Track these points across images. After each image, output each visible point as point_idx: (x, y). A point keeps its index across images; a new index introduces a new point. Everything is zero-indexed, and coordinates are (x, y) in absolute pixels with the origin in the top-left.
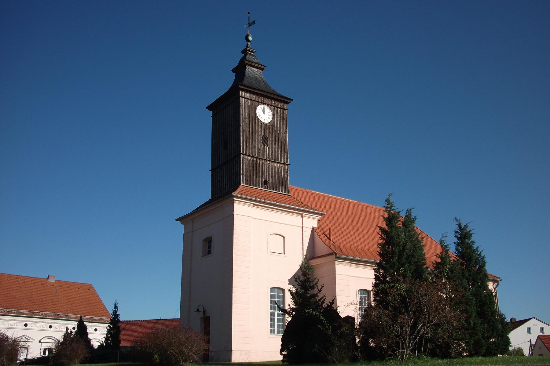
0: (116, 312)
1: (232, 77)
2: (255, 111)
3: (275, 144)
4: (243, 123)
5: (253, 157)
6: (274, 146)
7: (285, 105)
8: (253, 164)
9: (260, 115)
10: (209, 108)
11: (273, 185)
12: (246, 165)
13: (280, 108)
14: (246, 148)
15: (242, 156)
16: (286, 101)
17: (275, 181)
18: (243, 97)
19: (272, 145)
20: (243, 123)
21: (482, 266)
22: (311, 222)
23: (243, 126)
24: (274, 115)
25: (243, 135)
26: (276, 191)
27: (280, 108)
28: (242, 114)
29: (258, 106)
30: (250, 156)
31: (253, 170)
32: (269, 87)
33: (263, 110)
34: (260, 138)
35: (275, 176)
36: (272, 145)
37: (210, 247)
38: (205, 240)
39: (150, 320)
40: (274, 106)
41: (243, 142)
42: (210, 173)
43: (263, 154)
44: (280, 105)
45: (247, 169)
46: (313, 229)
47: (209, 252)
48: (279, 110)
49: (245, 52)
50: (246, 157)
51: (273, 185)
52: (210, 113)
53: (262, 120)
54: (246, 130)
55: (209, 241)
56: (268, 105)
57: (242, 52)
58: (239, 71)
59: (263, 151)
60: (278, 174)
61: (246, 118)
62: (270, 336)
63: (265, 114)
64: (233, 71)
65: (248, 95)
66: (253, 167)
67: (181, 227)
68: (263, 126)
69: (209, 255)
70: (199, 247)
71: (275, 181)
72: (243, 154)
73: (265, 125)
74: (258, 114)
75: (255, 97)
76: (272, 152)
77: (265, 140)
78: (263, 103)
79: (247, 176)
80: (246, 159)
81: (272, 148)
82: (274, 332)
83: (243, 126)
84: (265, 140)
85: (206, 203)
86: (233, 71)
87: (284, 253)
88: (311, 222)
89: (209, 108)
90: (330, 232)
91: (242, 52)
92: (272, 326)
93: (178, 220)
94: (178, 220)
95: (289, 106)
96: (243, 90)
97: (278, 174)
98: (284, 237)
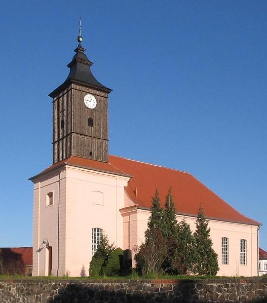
1: (66, 72)
16: (108, 91)
35: (98, 149)
44: (102, 94)
56: (93, 94)
57: (75, 51)
58: (72, 65)
63: (90, 101)
64: (69, 66)
65: (78, 87)
74: (85, 102)
75: (84, 89)
77: (91, 122)
78: (89, 93)
84: (91, 122)
86: (69, 66)
96: (74, 83)
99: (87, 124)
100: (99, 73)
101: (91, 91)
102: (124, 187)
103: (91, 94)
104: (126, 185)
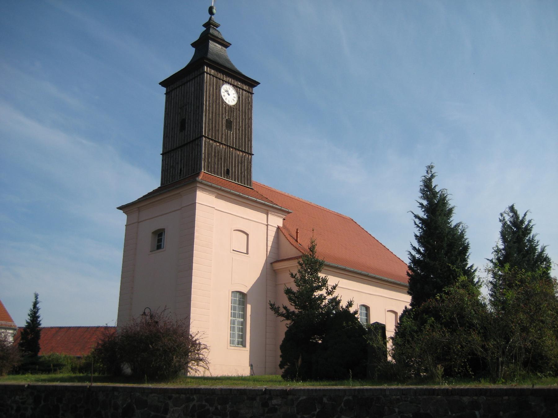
0: (35, 313)
1: (191, 52)
2: (220, 90)
3: (239, 130)
4: (206, 102)
5: (215, 141)
6: (238, 132)
7: (251, 89)
8: (215, 149)
9: (224, 96)
10: (163, 84)
11: (235, 175)
12: (208, 150)
13: (245, 91)
14: (209, 130)
15: (204, 139)
16: (252, 83)
17: (238, 171)
18: (207, 73)
19: (236, 131)
20: (206, 102)
21: (548, 267)
22: (276, 221)
23: (206, 105)
24: (239, 98)
25: (206, 115)
26: (238, 183)
27: (245, 91)
28: (206, 92)
29: (223, 84)
30: (212, 140)
31: (215, 155)
32: (234, 66)
33: (227, 91)
34: (224, 122)
35: (238, 166)
36: (236, 131)
37: (160, 241)
38: (155, 233)
39: (52, 328)
40: (240, 88)
41: (205, 123)
42: (159, 159)
43: (226, 140)
44: (246, 87)
45: (208, 154)
46: (278, 228)
47: (159, 247)
48: (244, 92)
49: (209, 25)
50: (208, 140)
51: (235, 175)
52: (164, 90)
53: (227, 102)
54: (209, 110)
55: (159, 234)
56: (234, 86)
57: (204, 26)
58: (201, 45)
59: (227, 136)
60: (241, 164)
61: (209, 97)
62: (229, 347)
63: (229, 95)
64: (193, 45)
65: (213, 71)
66: (215, 152)
67: (123, 217)
68: (227, 108)
69: (158, 251)
70: (146, 239)
71: (238, 171)
72: (205, 137)
73: (230, 107)
74: (222, 94)
75: (220, 75)
76: (236, 138)
77: (229, 124)
78: (229, 83)
79: (208, 162)
80: (209, 144)
81: (236, 134)
82: (233, 344)
83: (206, 105)
84: (229, 124)
85: (155, 192)
86: (193, 45)
87: (247, 253)
88: (276, 221)
89: (163, 84)
90: (297, 233)
91: (204, 26)
92: (232, 335)
93: (120, 208)
94: (120, 208)
95: (255, 90)
96: (208, 66)
97: (241, 164)
98: (247, 235)
99: (224, 127)
100: (236, 58)
101: (233, 81)
102: (416, 236)
103: (231, 84)
104: (281, 225)
